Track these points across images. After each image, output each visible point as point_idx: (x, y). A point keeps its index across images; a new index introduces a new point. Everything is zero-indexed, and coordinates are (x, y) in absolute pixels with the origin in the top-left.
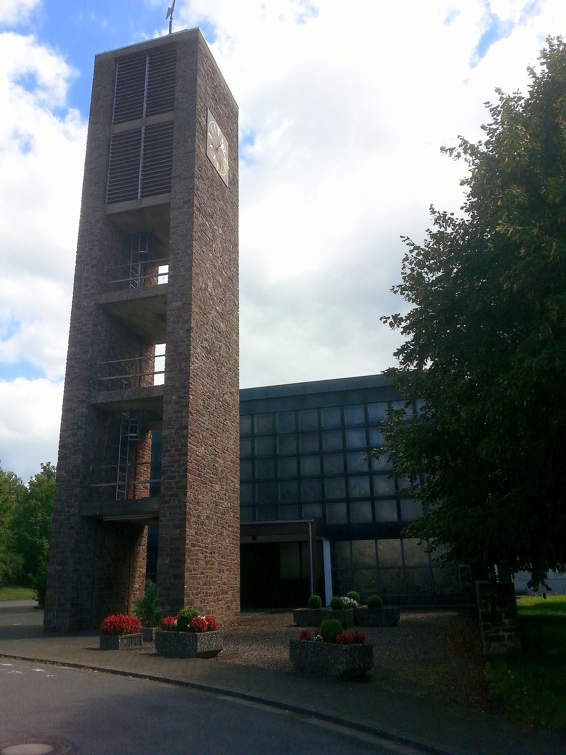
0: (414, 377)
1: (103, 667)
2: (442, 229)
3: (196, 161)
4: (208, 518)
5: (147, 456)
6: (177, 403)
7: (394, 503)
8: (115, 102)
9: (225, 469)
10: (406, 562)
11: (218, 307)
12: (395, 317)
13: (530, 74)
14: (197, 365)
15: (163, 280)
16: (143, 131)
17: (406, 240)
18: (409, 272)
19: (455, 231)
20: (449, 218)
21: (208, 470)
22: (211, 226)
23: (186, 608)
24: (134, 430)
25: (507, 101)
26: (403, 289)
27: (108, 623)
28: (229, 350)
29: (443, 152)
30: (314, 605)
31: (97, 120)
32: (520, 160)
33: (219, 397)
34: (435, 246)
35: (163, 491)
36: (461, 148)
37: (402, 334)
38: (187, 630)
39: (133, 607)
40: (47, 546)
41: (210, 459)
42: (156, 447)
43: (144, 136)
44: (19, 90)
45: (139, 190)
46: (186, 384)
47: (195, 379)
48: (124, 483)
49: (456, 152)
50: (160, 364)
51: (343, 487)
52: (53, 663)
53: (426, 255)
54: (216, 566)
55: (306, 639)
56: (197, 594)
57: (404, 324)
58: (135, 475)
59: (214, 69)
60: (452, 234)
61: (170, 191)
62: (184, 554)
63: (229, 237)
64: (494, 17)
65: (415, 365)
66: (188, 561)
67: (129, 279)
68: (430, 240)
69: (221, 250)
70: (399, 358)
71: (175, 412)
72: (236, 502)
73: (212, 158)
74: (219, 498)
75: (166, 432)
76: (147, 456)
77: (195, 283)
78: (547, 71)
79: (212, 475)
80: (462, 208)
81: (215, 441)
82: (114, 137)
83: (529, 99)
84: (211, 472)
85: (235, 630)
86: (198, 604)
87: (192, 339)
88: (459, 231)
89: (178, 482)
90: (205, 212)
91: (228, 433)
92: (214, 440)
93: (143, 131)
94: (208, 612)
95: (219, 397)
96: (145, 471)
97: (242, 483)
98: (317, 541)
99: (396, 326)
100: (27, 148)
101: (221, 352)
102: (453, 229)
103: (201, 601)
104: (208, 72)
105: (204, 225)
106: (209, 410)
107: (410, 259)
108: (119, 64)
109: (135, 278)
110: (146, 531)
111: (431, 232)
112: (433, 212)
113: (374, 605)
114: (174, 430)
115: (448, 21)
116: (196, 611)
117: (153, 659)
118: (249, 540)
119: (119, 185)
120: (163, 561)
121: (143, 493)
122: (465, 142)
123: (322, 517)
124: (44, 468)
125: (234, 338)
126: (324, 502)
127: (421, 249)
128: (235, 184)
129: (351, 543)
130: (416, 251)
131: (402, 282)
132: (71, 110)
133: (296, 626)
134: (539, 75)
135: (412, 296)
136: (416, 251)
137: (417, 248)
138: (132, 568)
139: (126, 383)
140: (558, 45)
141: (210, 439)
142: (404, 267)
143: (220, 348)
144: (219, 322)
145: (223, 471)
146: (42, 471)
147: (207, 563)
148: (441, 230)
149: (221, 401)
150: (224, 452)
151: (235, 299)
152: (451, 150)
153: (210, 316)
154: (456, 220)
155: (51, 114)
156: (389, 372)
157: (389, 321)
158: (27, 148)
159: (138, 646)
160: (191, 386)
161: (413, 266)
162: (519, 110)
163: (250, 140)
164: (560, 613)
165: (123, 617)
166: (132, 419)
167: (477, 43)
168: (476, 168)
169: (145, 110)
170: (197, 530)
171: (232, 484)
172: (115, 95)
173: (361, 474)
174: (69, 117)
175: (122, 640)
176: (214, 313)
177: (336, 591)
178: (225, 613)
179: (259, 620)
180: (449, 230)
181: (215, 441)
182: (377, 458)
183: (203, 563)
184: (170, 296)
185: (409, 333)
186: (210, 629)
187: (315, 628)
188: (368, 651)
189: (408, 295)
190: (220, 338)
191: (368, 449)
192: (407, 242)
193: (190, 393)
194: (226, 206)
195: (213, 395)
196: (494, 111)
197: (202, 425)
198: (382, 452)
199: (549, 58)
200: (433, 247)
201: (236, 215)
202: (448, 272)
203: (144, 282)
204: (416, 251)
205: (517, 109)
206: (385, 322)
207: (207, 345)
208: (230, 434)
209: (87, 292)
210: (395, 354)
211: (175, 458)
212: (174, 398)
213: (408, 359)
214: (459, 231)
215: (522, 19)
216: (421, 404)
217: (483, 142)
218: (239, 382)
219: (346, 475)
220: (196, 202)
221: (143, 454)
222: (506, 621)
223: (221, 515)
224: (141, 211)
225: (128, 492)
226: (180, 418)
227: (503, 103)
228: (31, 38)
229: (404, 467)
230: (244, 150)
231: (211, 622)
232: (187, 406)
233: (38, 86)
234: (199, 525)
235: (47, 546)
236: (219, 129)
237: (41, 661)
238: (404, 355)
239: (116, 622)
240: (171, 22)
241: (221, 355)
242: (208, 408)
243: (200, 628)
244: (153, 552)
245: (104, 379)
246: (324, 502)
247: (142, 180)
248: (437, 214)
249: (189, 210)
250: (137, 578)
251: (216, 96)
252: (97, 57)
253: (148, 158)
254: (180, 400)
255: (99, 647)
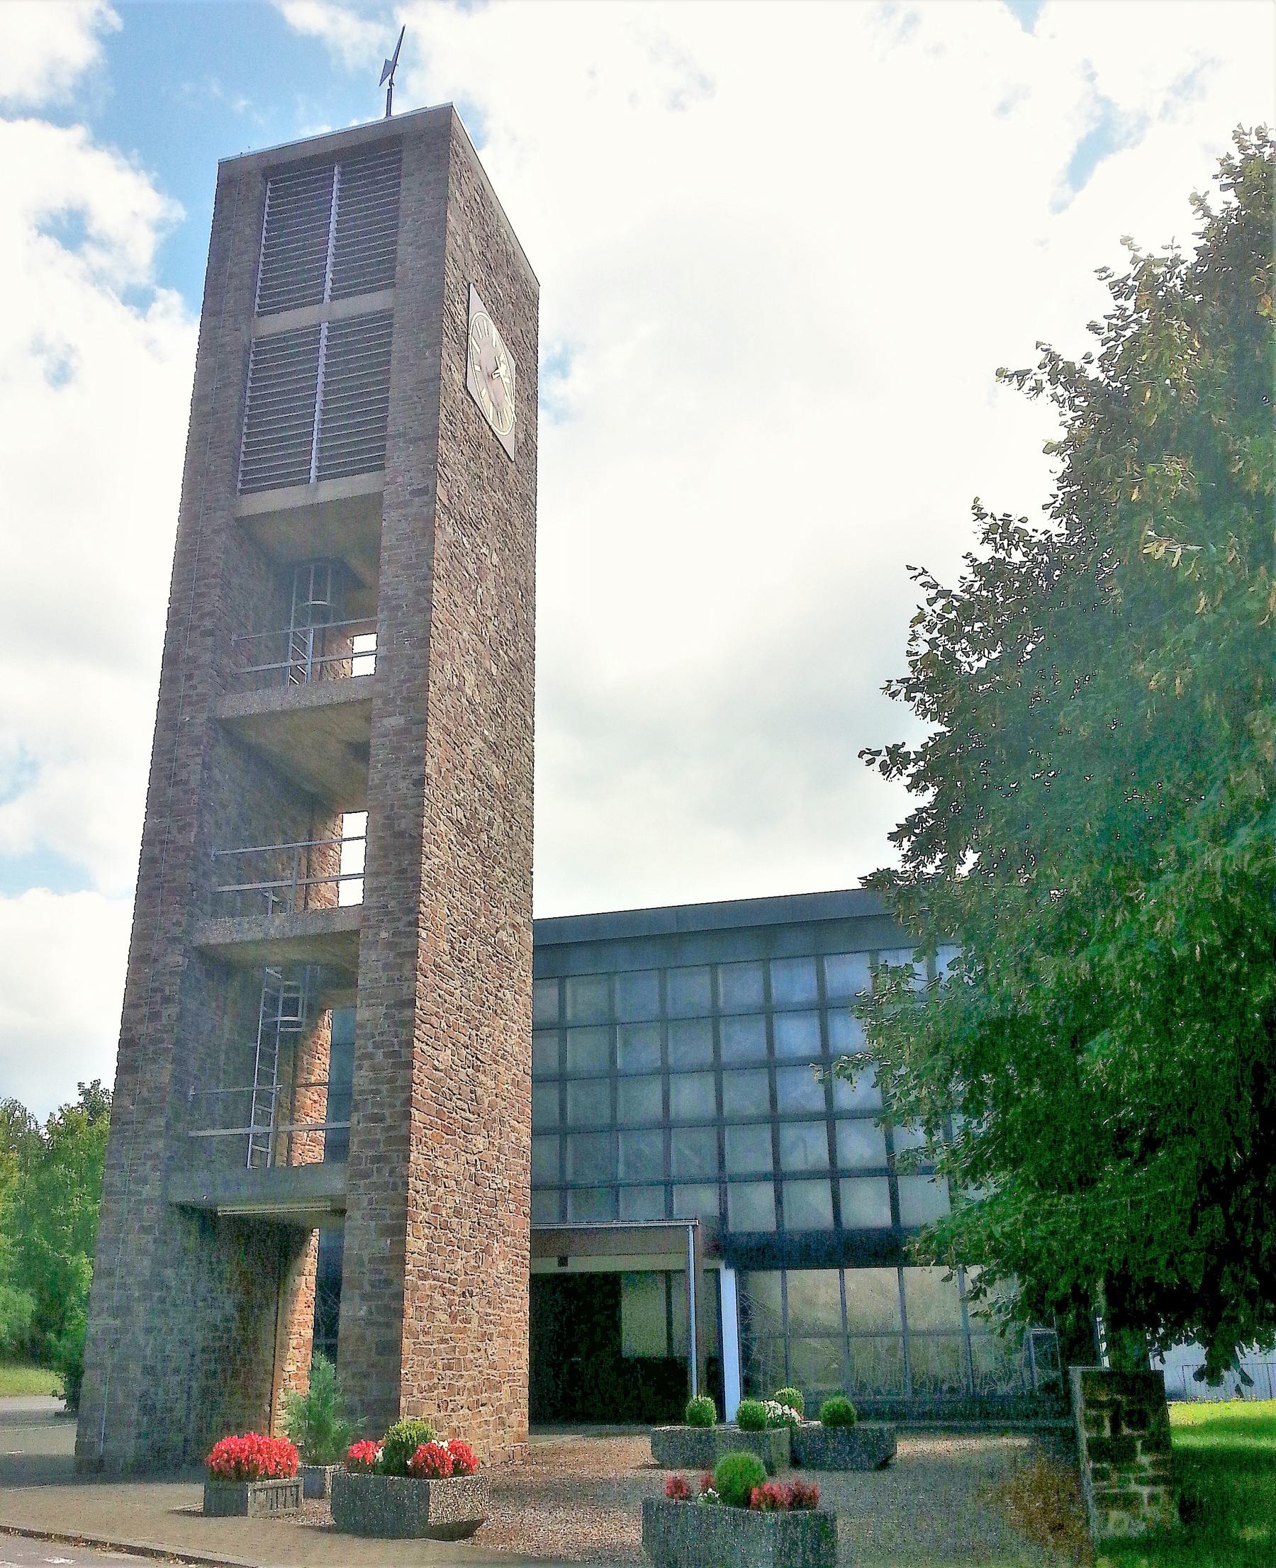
0: (935, 890)
1: (209, 1556)
2: (1001, 554)
3: (442, 400)
4: (457, 1213)
5: (320, 1067)
6: (390, 945)
7: (883, 1184)
8: (261, 267)
9: (499, 1100)
10: (910, 1322)
11: (488, 730)
12: (894, 751)
13: (1197, 210)
14: (436, 861)
15: (364, 667)
16: (325, 332)
17: (920, 574)
18: (923, 648)
19: (1030, 557)
20: (1017, 529)
21: (459, 1103)
22: (474, 546)
23: (405, 1420)
24: (291, 1008)
25: (1145, 267)
26: (911, 688)
27: (224, 1452)
28: (511, 827)
29: (1003, 379)
30: (699, 1420)
31: (215, 587)
32: (1178, 397)
33: (486, 936)
34: (984, 593)
35: (355, 1148)
36: (1043, 370)
37: (910, 791)
38: (405, 1472)
39: (282, 1418)
40: (88, 1272)
41: (464, 1078)
42: (342, 1047)
43: (331, 276)
44: (49, 245)
45: (314, 464)
46: (411, 905)
47: (432, 892)
48: (267, 1129)
49: (1033, 380)
50: (353, 857)
51: (769, 1147)
52: (94, 1544)
53: (967, 610)
54: (474, 1324)
55: (681, 1498)
56: (431, 1389)
57: (912, 769)
58: (292, 1113)
59: (485, 196)
60: (1022, 564)
61: (382, 467)
62: (400, 1296)
63: (515, 573)
64: (1106, 103)
65: (937, 863)
66: (410, 1311)
67: (284, 664)
68: (972, 577)
69: (497, 601)
70: (900, 846)
71: (387, 966)
72: (522, 1178)
73: (480, 394)
74: (484, 1167)
75: (363, 1014)
76: (320, 1067)
77: (435, 675)
78: (1235, 203)
79: (468, 1115)
80: (1045, 507)
81: (477, 1035)
82: (257, 345)
83: (1197, 264)
84: (465, 1107)
85: (515, 1473)
86: (431, 1411)
87: (426, 802)
88: (1040, 558)
89: (391, 1128)
90: (460, 514)
91: (507, 1018)
92: (474, 1033)
93: (325, 332)
94: (455, 1432)
95: (486, 936)
96: (315, 1102)
97: (536, 1133)
98: (706, 1271)
99: (894, 771)
100: (61, 376)
101: (493, 833)
102: (1025, 554)
103: (439, 1406)
104: (473, 202)
105: (457, 544)
106: (463, 964)
107: (927, 619)
108: (274, 183)
109: (299, 662)
110: (314, 1241)
111: (976, 560)
112: (980, 516)
113: (838, 1419)
114: (382, 1010)
115: (1003, 109)
116: (428, 1427)
117: (326, 1539)
118: (550, 1266)
119: (266, 460)
120: (351, 1310)
121: (311, 1154)
122: (1053, 358)
123: (718, 1215)
124: (85, 1093)
125: (524, 800)
126: (722, 1180)
127: (954, 596)
128: (528, 455)
129: (784, 1277)
130: (942, 602)
131: (907, 672)
132: (162, 292)
133: (661, 1467)
134: (1216, 212)
135: (932, 704)
136: (943, 602)
137: (945, 594)
138: (279, 1326)
139: (276, 899)
140: (1258, 147)
141: (464, 1031)
142: (914, 637)
143: (490, 824)
144: (489, 763)
145: (492, 1106)
146: (81, 1101)
147: (453, 1317)
148: (997, 556)
149: (490, 944)
150: (496, 1062)
151: (527, 714)
152: (1022, 375)
153: (469, 751)
154: (1031, 533)
155: (117, 301)
156: (879, 879)
157: (879, 759)
158: (61, 376)
159: (292, 1510)
160: (423, 909)
161: (936, 634)
162: (1175, 286)
163: (562, 367)
164: (1264, 1443)
165: (257, 1438)
166: (288, 983)
167: (1067, 158)
168: (1078, 418)
169: (329, 285)
170: (430, 1241)
171: (513, 1137)
172: (263, 250)
173: (809, 1118)
174: (157, 307)
175: (256, 1493)
176: (478, 743)
177: (749, 1387)
178: (493, 1434)
179: (572, 1451)
180: (1017, 557)
181: (477, 1035)
182: (849, 1078)
183: (444, 1317)
184: (378, 702)
185: (925, 789)
186: (457, 1471)
187: (703, 1472)
188: (824, 1528)
189: (922, 701)
190: (491, 800)
191: (825, 1059)
192: (922, 579)
193: (421, 924)
194: (508, 502)
195: (473, 930)
196: (1120, 289)
197: (448, 998)
198: (859, 1065)
199: (1241, 174)
200: (978, 593)
201: (531, 524)
202: (1012, 657)
203: (322, 671)
204: (943, 602)
205: (1171, 284)
206: (870, 762)
207: (461, 815)
208: (511, 1019)
209: (191, 692)
210: (892, 837)
211: (384, 1074)
212: (384, 935)
213: (920, 851)
214: (1040, 558)
215: (1167, 107)
216: (945, 957)
217: (1096, 355)
218: (532, 902)
219: (774, 1119)
220: (440, 492)
221: (311, 1064)
222: (1144, 1460)
223: (486, 1208)
224: (316, 510)
225: (274, 1149)
226: (397, 982)
227: (1138, 269)
228: (78, 133)
229: (912, 1098)
230: (548, 387)
231: (461, 1455)
232: (414, 954)
233: (87, 238)
234: (436, 1228)
235: (88, 1272)
236: (495, 332)
237: (67, 1539)
238: (913, 838)
239: (242, 1450)
240: (390, 91)
241: (491, 838)
242: (460, 961)
243: (435, 1469)
244: (330, 1287)
245: (226, 888)
246: (722, 1180)
247: (321, 440)
248: (988, 520)
249: (425, 510)
250: (291, 1350)
251: (489, 256)
252: (223, 165)
253: (334, 393)
254: (397, 940)
255: (199, 1507)
